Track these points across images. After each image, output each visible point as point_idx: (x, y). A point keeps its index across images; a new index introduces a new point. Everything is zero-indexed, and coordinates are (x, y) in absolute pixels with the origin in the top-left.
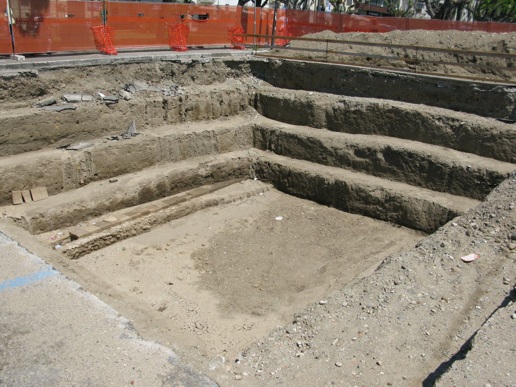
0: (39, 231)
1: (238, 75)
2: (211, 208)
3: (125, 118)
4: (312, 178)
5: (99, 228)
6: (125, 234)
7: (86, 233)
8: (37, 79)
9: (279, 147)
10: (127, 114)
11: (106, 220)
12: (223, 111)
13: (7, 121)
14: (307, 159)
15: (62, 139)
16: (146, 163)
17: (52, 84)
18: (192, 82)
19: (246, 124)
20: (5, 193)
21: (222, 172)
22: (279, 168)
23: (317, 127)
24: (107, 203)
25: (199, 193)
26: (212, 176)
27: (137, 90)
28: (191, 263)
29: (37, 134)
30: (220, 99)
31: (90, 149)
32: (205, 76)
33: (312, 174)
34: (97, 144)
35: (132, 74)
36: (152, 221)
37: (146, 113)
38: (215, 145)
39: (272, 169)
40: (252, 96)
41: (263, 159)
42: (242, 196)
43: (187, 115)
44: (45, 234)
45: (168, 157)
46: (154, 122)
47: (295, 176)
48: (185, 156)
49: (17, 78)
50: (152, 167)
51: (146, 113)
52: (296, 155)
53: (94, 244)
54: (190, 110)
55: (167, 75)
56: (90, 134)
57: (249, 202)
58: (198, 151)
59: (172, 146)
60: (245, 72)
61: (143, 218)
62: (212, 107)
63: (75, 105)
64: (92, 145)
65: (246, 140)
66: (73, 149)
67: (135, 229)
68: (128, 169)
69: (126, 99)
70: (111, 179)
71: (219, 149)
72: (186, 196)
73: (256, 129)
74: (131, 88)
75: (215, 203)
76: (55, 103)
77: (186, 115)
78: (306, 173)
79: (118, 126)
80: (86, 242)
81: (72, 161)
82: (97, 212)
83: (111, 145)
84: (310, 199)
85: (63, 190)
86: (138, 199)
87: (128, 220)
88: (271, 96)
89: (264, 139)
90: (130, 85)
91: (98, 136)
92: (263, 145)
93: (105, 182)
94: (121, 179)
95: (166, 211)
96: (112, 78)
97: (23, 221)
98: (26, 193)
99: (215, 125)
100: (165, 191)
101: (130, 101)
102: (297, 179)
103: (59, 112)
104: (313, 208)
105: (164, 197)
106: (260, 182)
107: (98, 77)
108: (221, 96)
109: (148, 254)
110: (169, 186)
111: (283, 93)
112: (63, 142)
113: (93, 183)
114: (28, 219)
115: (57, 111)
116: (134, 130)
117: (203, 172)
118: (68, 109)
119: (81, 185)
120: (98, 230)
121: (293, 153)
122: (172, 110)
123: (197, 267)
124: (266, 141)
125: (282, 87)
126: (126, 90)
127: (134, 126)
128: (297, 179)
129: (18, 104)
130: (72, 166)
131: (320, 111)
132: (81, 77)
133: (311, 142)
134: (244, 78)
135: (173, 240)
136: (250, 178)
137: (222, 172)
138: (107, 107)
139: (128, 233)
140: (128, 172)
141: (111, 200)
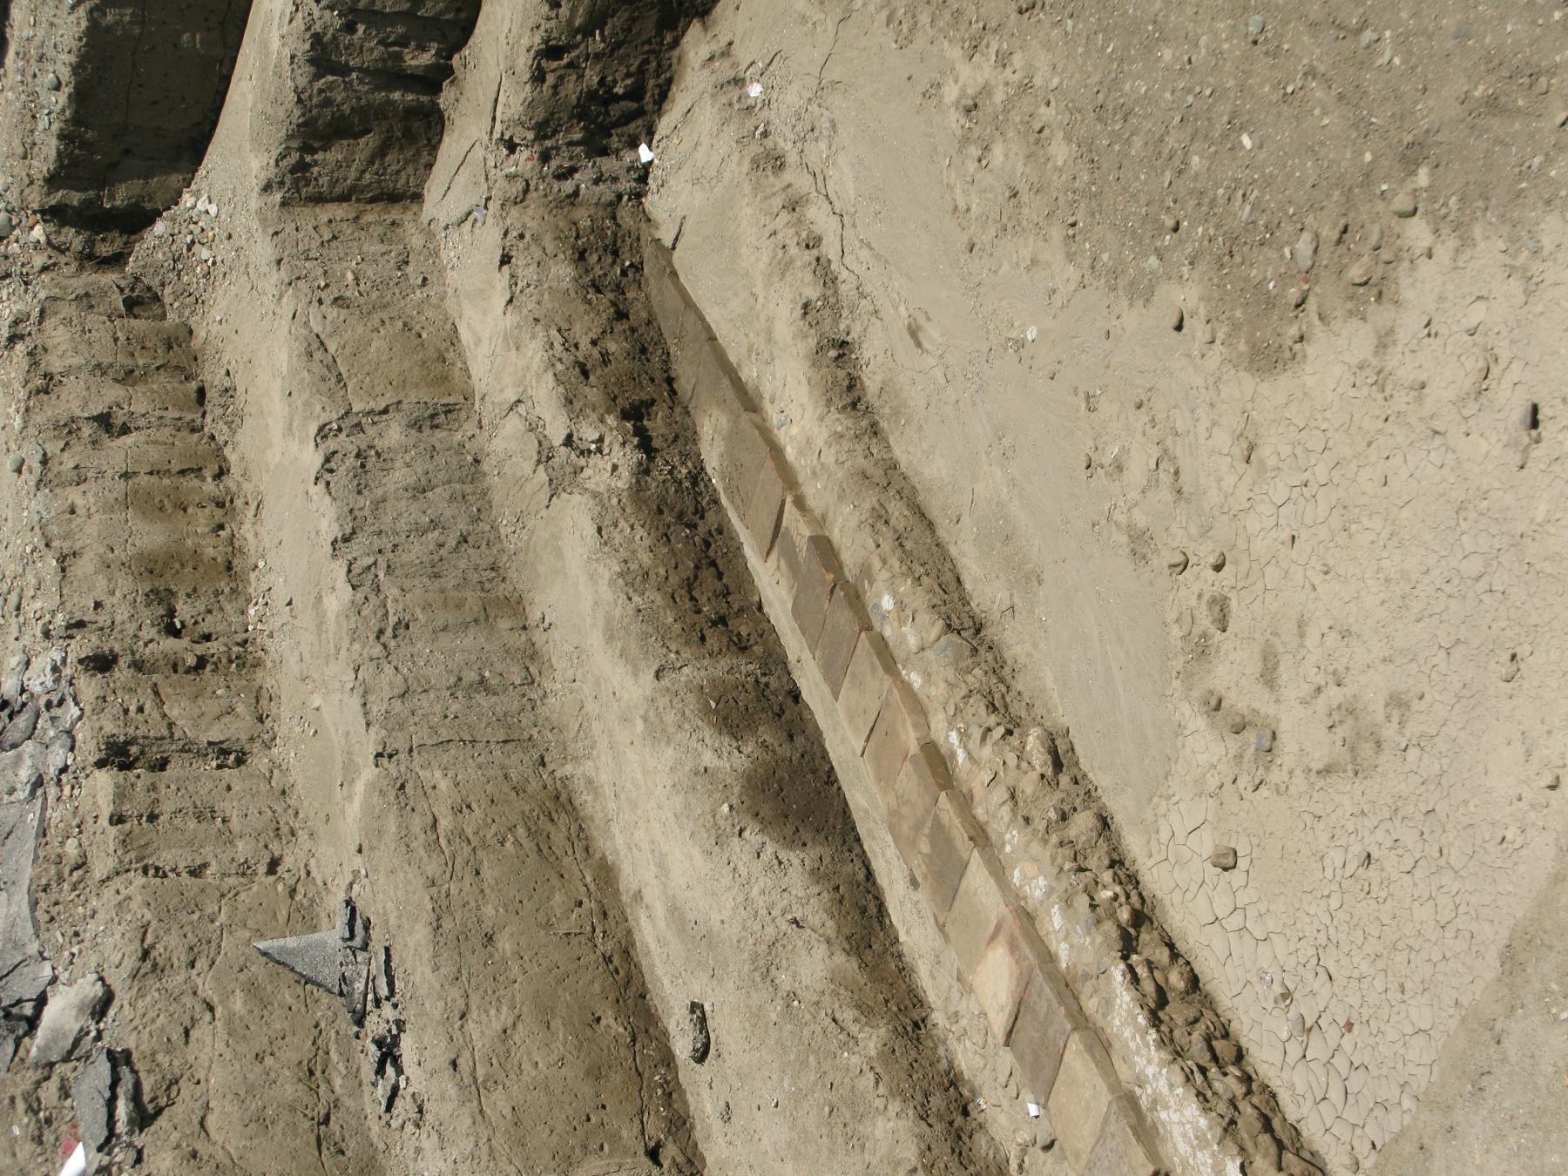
2: (871, 382)
3: (238, 1004)
5: (1075, 1044)
6: (1107, 876)
7: (1121, 1128)
10: (208, 990)
12: (172, 413)
16: (559, 838)
19: (262, 250)
21: (605, 359)
24: (873, 1039)
25: (769, 473)
26: (635, 414)
27: (33, 948)
28: (1334, 353)
36: (992, 720)
37: (196, 872)
39: (587, 31)
40: (61, 249)
41: (515, 100)
42: (777, 202)
43: (204, 628)
45: (509, 702)
46: (256, 822)
48: (496, 599)
50: (584, 798)
51: (196, 872)
53: (1205, 1059)
54: (171, 613)
57: (816, 151)
58: (462, 526)
59: (437, 674)
61: (975, 779)
62: (143, 480)
65: (375, 248)
67: (1064, 817)
68: (609, 947)
69: (101, 1007)
70: (682, 1047)
71: (443, 405)
72: (790, 555)
73: (296, 183)
75: (838, 355)
79: (298, 1049)
80: (1192, 1109)
82: (937, 1102)
83: (443, 1060)
86: (827, 852)
87: (998, 871)
88: (62, 98)
92: (409, 137)
93: (703, 1093)
94: (673, 988)
95: (913, 641)
99: (277, 447)
100: (762, 691)
101: (117, 980)
105: (795, 695)
106: (664, 126)
108: (68, 429)
109: (1269, 677)
110: (724, 663)
116: (323, 944)
117: (613, 466)
120: (1089, 1049)
122: (174, 713)
123: (1375, 289)
126: (33, 1023)
127: (291, 942)
135: (1140, 544)
136: (638, 196)
137: (605, 359)
138: (162, 1122)
140: (627, 952)
141: (848, 1015)
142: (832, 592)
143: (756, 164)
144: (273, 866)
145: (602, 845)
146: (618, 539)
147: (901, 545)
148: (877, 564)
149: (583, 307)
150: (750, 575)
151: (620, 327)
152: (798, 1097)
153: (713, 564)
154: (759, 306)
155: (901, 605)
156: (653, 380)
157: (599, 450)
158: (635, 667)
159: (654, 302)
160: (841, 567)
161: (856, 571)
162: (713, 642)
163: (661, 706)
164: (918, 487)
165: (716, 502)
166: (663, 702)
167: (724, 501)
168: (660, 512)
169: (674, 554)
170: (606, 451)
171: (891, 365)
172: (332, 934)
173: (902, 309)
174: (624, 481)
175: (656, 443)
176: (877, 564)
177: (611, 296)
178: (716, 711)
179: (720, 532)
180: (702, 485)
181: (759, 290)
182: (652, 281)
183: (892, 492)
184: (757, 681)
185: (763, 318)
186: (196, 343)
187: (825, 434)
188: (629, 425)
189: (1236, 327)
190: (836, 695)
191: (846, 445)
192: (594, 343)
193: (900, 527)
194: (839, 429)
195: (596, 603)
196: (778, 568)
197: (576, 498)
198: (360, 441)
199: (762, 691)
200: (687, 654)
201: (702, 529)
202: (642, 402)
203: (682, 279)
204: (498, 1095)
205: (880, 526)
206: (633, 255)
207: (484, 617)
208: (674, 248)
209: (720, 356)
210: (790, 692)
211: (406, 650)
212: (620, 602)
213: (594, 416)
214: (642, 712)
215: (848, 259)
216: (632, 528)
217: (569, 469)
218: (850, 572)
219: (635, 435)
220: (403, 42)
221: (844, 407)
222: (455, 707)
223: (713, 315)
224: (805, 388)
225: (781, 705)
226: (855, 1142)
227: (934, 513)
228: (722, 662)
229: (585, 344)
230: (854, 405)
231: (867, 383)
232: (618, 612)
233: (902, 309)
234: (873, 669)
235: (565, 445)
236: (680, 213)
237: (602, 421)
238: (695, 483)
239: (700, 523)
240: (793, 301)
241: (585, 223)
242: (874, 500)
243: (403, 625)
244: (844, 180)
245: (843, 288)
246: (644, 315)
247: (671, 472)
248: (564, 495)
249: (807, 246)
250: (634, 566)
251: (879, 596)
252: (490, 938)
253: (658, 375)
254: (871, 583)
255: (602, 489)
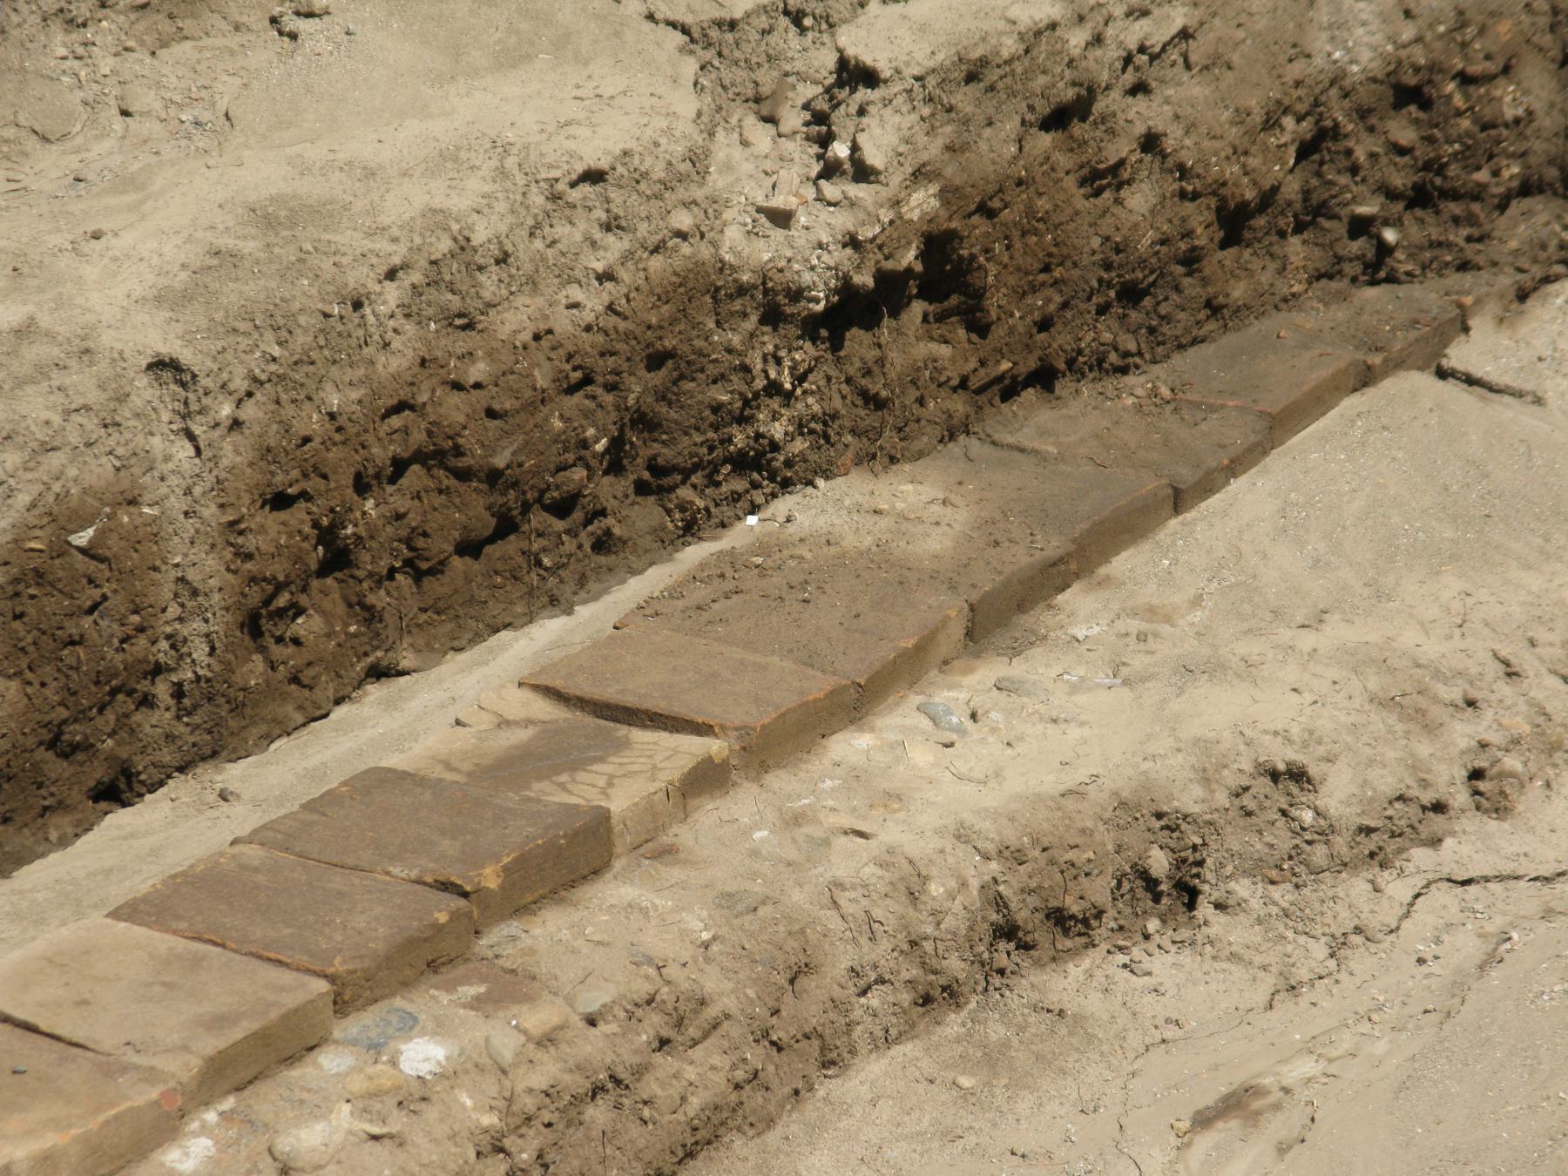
2: (1079, 981)
26: (942, 274)
100: (129, 687)
105: (118, 790)
110: (208, 568)
137: (1103, 179)
142: (445, 886)
146: (568, 233)
147: (596, 1091)
148: (539, 1018)
149: (1254, 103)
150: (477, 638)
151: (1200, 217)
153: (506, 526)
154: (1286, 634)
155: (415, 1097)
156: (1044, 325)
157: (830, 170)
158: (186, 297)
159: (1275, 322)
160: (522, 910)
161: (511, 957)
162: (273, 532)
163: (71, 379)
164: (772, 1138)
165: (690, 529)
166: (84, 384)
167: (694, 554)
168: (656, 361)
169: (530, 407)
170: (831, 190)
171: (1135, 1040)
173: (1307, 1067)
174: (747, 248)
175: (858, 342)
176: (539, 1018)
177: (1292, 189)
178: (61, 550)
179: (603, 544)
180: (739, 485)
181: (1336, 633)
182: (1340, 313)
183: (755, 1055)
184: (157, 670)
185: (1251, 648)
187: (917, 847)
188: (909, 257)
190: (128, 912)
191: (888, 911)
192: (1150, 143)
193: (649, 1086)
194: (935, 889)
195: (370, 173)
196: (504, 723)
197: (686, 104)
199: (129, 687)
200: (233, 453)
201: (608, 489)
202: (979, 295)
203: (1351, 404)
205: (655, 1023)
206: (1414, 252)
208: (1442, 374)
209: (1127, 526)
210: (128, 773)
212: (383, 245)
213: (932, 149)
214: (45, 321)
215: (1445, 897)
216: (606, 277)
217: (767, 79)
218: (506, 940)
219: (881, 276)
221: (1000, 903)
223: (1248, 498)
224: (1050, 782)
225: (86, 747)
228: (212, 563)
229: (1145, 114)
230: (1008, 932)
231: (1075, 970)
232: (349, 239)
233: (1307, 1067)
234: (217, 1022)
235: (843, 63)
236: (1553, 387)
237: (920, 175)
238: (743, 463)
239: (625, 484)
240: (1312, 737)
241: (1509, 100)
242: (730, 1004)
245: (1356, 887)
246: (1239, 292)
247: (773, 388)
248: (690, 66)
249: (1476, 775)
250: (489, 285)
251: (440, 1029)
253: (1061, 340)
254: (477, 1004)
255: (717, 181)
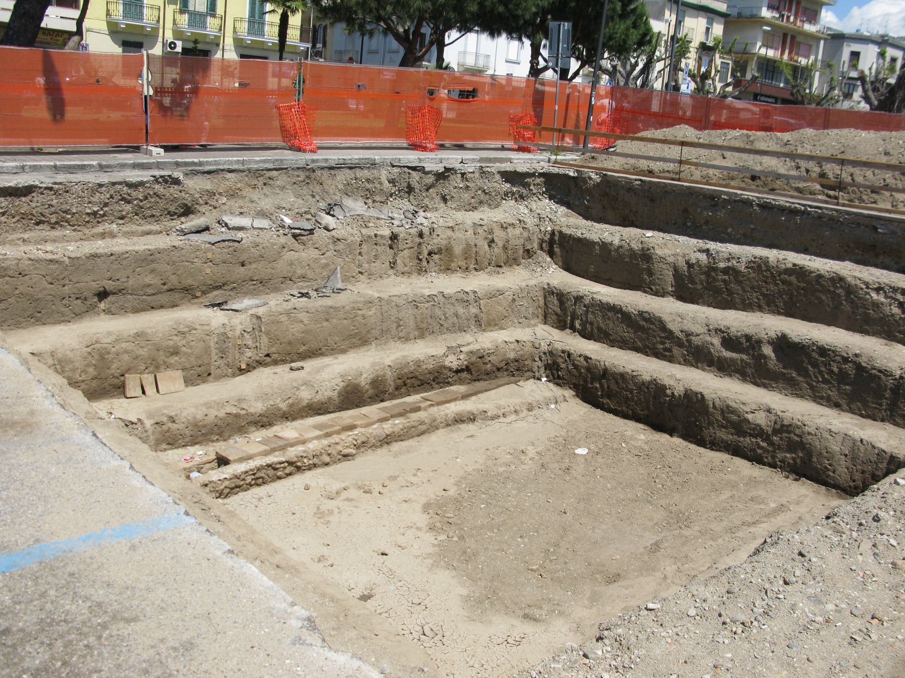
0: (164, 446)
1: (522, 197)
2: (463, 426)
3: (324, 261)
4: (643, 383)
6: (311, 462)
7: (244, 455)
8: (180, 188)
9: (588, 326)
10: (328, 254)
11: (280, 434)
12: (494, 258)
13: (127, 255)
14: (637, 350)
15: (215, 290)
16: (354, 340)
17: (205, 197)
18: (442, 205)
19: (533, 282)
20: (114, 377)
21: (485, 363)
22: (587, 362)
23: (656, 294)
24: (283, 406)
25: (443, 399)
26: (468, 369)
27: (348, 215)
28: (422, 520)
29: (173, 280)
30: (490, 236)
31: (261, 311)
32: (466, 196)
33: (643, 377)
34: (272, 303)
35: (341, 186)
36: (359, 442)
37: (360, 254)
38: (476, 316)
39: (573, 365)
41: (559, 346)
42: (518, 408)
44: (176, 451)
45: (394, 332)
46: (373, 270)
47: (614, 378)
48: (423, 332)
49: (148, 185)
50: (365, 348)
51: (360, 254)
52: (618, 341)
53: (257, 476)
54: (435, 254)
55: (399, 191)
56: (262, 285)
57: (531, 419)
58: (446, 325)
60: (535, 191)
61: (343, 436)
62: (474, 249)
63: (240, 235)
64: (265, 304)
65: (531, 310)
66: (232, 310)
67: (329, 455)
70: (293, 365)
71: (482, 323)
72: (420, 402)
73: (550, 292)
74: (337, 211)
75: (471, 418)
76: (207, 229)
77: (428, 262)
78: (634, 374)
79: (310, 274)
80: (243, 470)
81: (228, 329)
82: (265, 419)
84: (638, 420)
85: (210, 378)
86: (337, 402)
87: (318, 438)
89: (562, 311)
90: (335, 205)
91: (276, 290)
92: (560, 321)
93: (282, 369)
96: (305, 191)
97: (139, 426)
98: (148, 379)
99: (479, 282)
102: (617, 383)
103: (213, 244)
104: (642, 437)
105: (382, 401)
106: (551, 385)
107: (283, 188)
108: (491, 232)
109: (348, 500)
110: (392, 383)
111: (600, 232)
112: (216, 295)
113: (262, 369)
114: (148, 423)
115: (209, 243)
117: (452, 361)
118: (228, 240)
119: (242, 371)
120: (265, 451)
121: (612, 338)
123: (432, 528)
124: (565, 314)
125: (599, 221)
126: (328, 214)
127: (339, 275)
128: (617, 383)
129: (147, 227)
130: (228, 338)
131: (664, 266)
132: (254, 187)
133: (645, 319)
134: (533, 203)
135: (393, 478)
136: (534, 377)
137: (485, 363)
138: (294, 240)
139: (316, 461)
140: (322, 354)
141: (291, 401)
143: (530, 404)
144: (361, 273)
145: (352, 351)
152: (272, 388)
155: (395, 425)
162: (398, 381)
172: (340, 285)
174: (447, 364)
175: (459, 374)
186: (515, 266)
189: (438, 501)
198: (472, 301)
204: (286, 318)
207: (418, 328)
211: (410, 307)
220: (581, 320)
222: (393, 318)
226: (257, 399)
227: (422, 437)
241: (526, 363)
243: (417, 307)
244: (520, 424)
252: (327, 320)
